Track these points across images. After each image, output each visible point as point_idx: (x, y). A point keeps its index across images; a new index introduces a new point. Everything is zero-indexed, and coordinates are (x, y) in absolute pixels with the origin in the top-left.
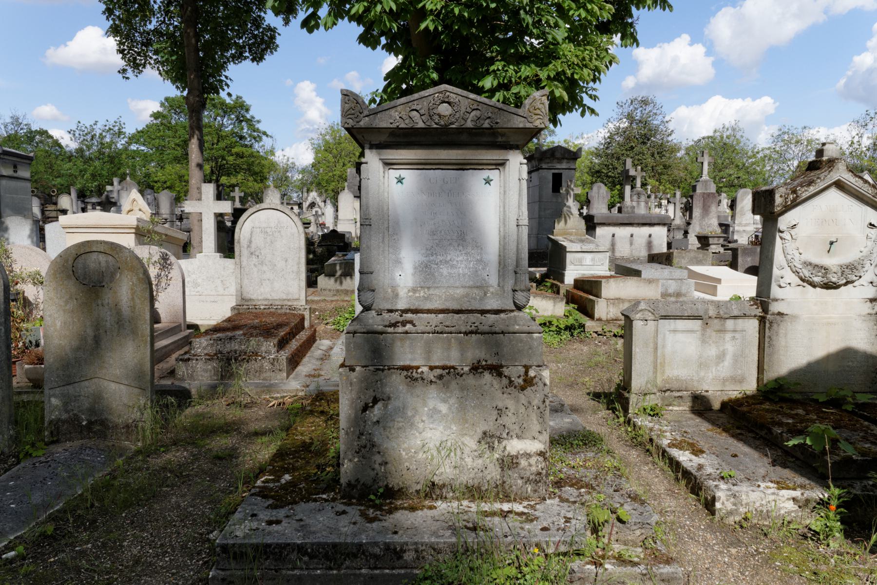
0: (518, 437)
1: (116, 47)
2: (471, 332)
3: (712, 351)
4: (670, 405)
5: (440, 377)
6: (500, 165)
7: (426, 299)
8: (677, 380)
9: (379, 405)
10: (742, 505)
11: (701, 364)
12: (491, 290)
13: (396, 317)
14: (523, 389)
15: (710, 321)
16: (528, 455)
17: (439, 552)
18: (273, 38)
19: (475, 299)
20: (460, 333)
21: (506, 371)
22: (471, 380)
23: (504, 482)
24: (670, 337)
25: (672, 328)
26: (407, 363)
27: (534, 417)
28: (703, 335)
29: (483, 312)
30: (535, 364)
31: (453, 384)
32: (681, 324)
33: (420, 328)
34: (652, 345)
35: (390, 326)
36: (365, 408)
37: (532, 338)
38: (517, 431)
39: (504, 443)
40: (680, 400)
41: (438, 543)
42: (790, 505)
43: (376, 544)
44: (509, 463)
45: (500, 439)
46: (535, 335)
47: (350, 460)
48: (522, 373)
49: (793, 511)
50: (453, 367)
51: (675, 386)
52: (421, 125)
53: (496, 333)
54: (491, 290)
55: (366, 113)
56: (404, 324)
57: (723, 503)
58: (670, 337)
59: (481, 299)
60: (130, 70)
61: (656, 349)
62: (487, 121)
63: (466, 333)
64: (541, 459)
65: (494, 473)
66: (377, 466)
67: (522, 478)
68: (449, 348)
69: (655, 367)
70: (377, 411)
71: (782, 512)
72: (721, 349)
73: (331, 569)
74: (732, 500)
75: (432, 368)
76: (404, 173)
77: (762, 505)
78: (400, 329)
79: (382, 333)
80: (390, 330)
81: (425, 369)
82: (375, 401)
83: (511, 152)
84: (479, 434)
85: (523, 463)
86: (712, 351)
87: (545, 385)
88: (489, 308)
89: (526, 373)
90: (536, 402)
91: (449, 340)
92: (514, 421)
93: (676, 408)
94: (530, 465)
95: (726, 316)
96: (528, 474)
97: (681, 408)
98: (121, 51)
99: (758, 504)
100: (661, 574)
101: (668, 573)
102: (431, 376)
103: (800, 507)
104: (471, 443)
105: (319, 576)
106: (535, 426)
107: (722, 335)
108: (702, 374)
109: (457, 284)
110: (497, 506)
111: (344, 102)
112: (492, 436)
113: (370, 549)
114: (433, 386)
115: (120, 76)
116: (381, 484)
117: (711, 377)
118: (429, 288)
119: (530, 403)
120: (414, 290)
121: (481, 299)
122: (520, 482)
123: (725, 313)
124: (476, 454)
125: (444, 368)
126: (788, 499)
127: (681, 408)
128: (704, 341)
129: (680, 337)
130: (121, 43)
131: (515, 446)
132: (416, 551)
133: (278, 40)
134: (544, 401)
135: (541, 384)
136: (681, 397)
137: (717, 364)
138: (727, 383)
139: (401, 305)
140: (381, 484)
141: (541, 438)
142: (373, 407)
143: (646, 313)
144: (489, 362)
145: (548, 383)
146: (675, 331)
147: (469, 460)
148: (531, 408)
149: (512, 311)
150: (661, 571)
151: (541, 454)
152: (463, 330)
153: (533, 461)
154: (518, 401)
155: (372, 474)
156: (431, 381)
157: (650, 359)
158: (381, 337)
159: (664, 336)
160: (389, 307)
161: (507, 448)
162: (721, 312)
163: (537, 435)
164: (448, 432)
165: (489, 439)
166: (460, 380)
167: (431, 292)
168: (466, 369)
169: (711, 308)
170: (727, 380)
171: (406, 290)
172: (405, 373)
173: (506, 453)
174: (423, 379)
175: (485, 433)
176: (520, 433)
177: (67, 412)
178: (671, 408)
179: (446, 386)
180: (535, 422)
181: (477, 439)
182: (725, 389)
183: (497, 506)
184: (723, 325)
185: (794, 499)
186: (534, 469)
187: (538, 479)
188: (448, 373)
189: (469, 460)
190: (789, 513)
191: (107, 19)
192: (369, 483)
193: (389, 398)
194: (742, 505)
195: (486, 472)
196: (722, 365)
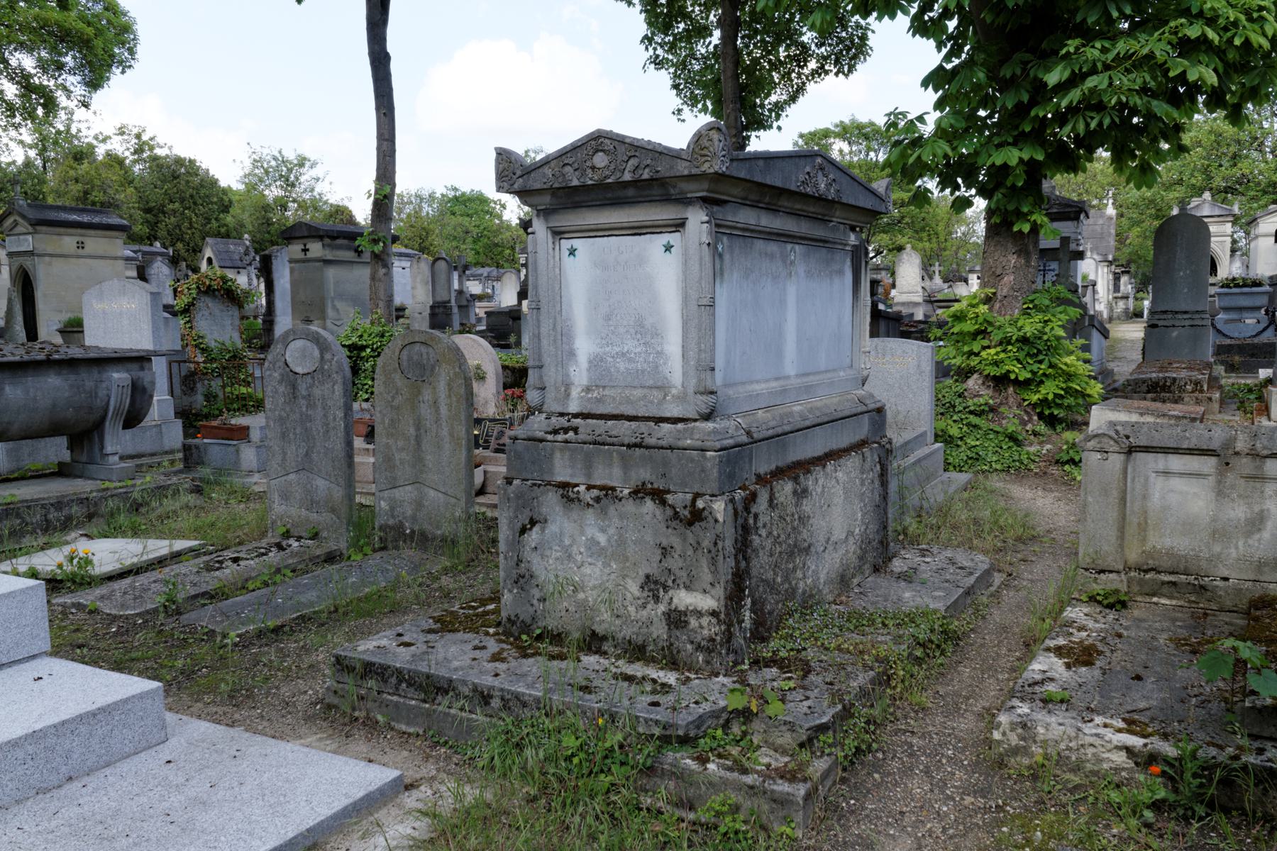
0: (687, 588)
1: (670, 82)
2: (635, 445)
3: (1238, 512)
4: (1154, 595)
5: (598, 500)
6: (679, 225)
7: (599, 401)
8: (1170, 553)
9: (536, 529)
10: (1035, 742)
11: (1214, 532)
12: (674, 391)
13: (563, 422)
14: (690, 523)
15: (1233, 461)
16: (699, 614)
17: (524, 705)
18: (864, 38)
19: (652, 402)
20: (623, 445)
21: (670, 498)
22: (630, 506)
23: (671, 644)
24: (1158, 486)
25: (1161, 467)
26: (568, 479)
27: (704, 563)
28: (1219, 482)
29: (659, 420)
30: (709, 492)
31: (612, 511)
32: (1176, 463)
33: (581, 437)
34: (1115, 493)
35: (550, 433)
36: (523, 531)
37: (704, 457)
38: (685, 579)
39: (670, 593)
40: (1173, 589)
41: (523, 694)
42: (1120, 758)
43: (464, 682)
44: (676, 619)
45: (666, 588)
46: (709, 454)
47: (510, 591)
48: (689, 504)
49: (1124, 769)
50: (613, 489)
51: (1166, 563)
52: (575, 183)
53: (662, 448)
54: (674, 391)
55: (519, 173)
56: (566, 431)
57: (1004, 734)
58: (1158, 486)
59: (660, 403)
60: (686, 109)
61: (1123, 500)
62: (647, 170)
63: (629, 446)
64: (714, 621)
65: (660, 630)
66: (535, 602)
67: (692, 643)
68: (610, 465)
69: (1122, 530)
70: (534, 536)
71: (1105, 766)
72: (1257, 509)
73: (425, 701)
74: (1020, 731)
75: (589, 488)
76: (577, 243)
77: (1069, 749)
78: (560, 437)
79: (541, 441)
80: (550, 437)
81: (582, 488)
82: (533, 523)
83: (690, 208)
84: (641, 579)
85: (693, 622)
86: (1238, 512)
87: (716, 521)
88: (668, 415)
89: (694, 501)
90: (706, 543)
91: (611, 453)
92: (680, 565)
93: (1163, 601)
94: (701, 627)
95: (1265, 452)
96: (699, 638)
97: (1174, 602)
98: (676, 87)
99: (1063, 746)
100: (773, 791)
101: (781, 793)
102: (588, 497)
103: (1137, 764)
104: (633, 588)
105: (414, 707)
106: (707, 576)
107: (1258, 485)
108: (1217, 549)
109: (636, 383)
110: (653, 673)
111: (498, 162)
112: (656, 582)
113: (460, 688)
114: (591, 510)
115: (675, 117)
116: (540, 624)
117: (1234, 555)
118: (604, 387)
119: (698, 543)
120: (588, 389)
121: (660, 403)
122: (689, 647)
123: (1264, 448)
124: (640, 602)
125: (602, 488)
126: (1118, 748)
127: (1174, 602)
128: (1221, 493)
129: (1176, 483)
130: (676, 76)
131: (684, 599)
132: (502, 699)
133: (872, 40)
134: (716, 544)
135: (710, 520)
136: (1174, 584)
137: (1248, 534)
138: (1266, 569)
139: (573, 407)
140: (540, 624)
141: (713, 592)
142: (531, 529)
143: (1105, 440)
144: (656, 486)
145: (721, 520)
146: (1166, 473)
147: (632, 609)
148: (700, 551)
149: (695, 420)
150: (775, 787)
151: (714, 614)
152: (626, 442)
153: (705, 621)
154: (685, 540)
155: (531, 610)
156: (588, 505)
157: (1113, 515)
158: (541, 445)
159: (1147, 479)
160: (560, 409)
161: (675, 600)
162: (1258, 445)
163: (708, 587)
164: (607, 571)
165: (654, 586)
166: (618, 505)
167: (607, 392)
168: (626, 491)
169: (1241, 437)
170: (1266, 564)
171: (579, 389)
172: (561, 491)
173: (673, 607)
174: (579, 500)
175: (648, 577)
176: (688, 583)
177: (393, 516)
178: (1155, 599)
179: (604, 512)
180: (706, 570)
181: (639, 584)
182: (1262, 579)
183: (653, 673)
184: (1260, 468)
185: (1129, 750)
186: (705, 632)
187: (709, 648)
188: (606, 495)
189: (632, 609)
190: (1117, 770)
191: (647, 49)
192: (529, 621)
193: (546, 521)
194: (1035, 742)
195: (652, 629)
196: (1257, 536)
